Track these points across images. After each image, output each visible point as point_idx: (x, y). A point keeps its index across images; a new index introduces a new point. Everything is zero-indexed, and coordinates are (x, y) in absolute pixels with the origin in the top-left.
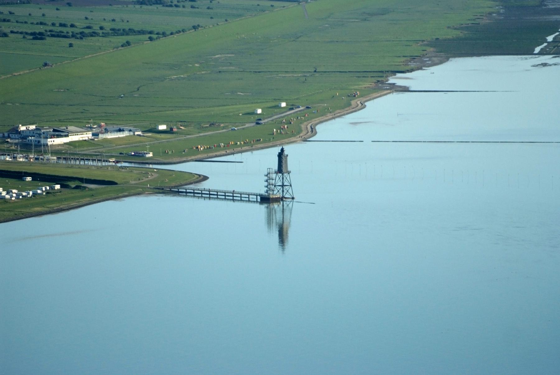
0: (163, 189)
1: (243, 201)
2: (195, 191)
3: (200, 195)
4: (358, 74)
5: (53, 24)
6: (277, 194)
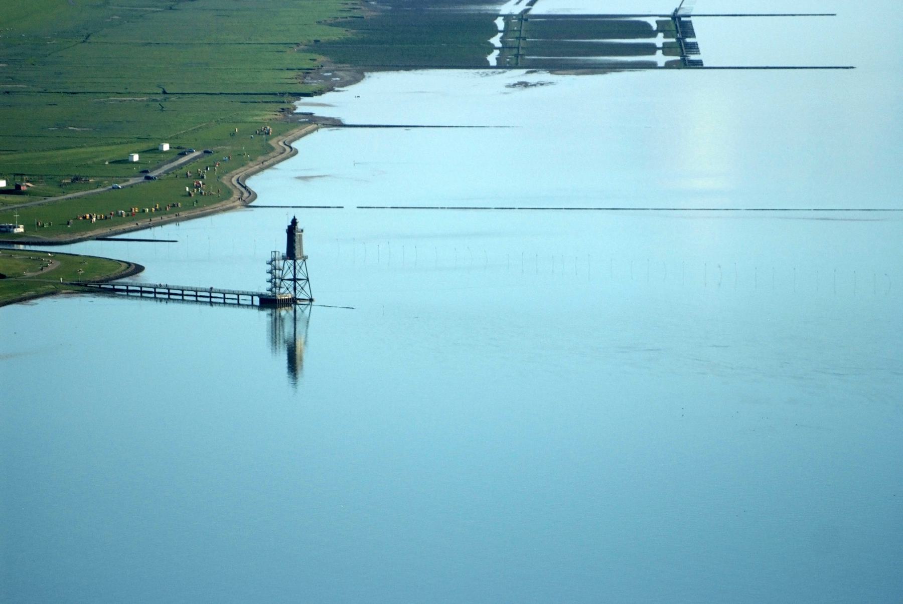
0: (86, 285)
2: (144, 289)
3: (153, 295)
4: (245, 98)
6: (285, 292)
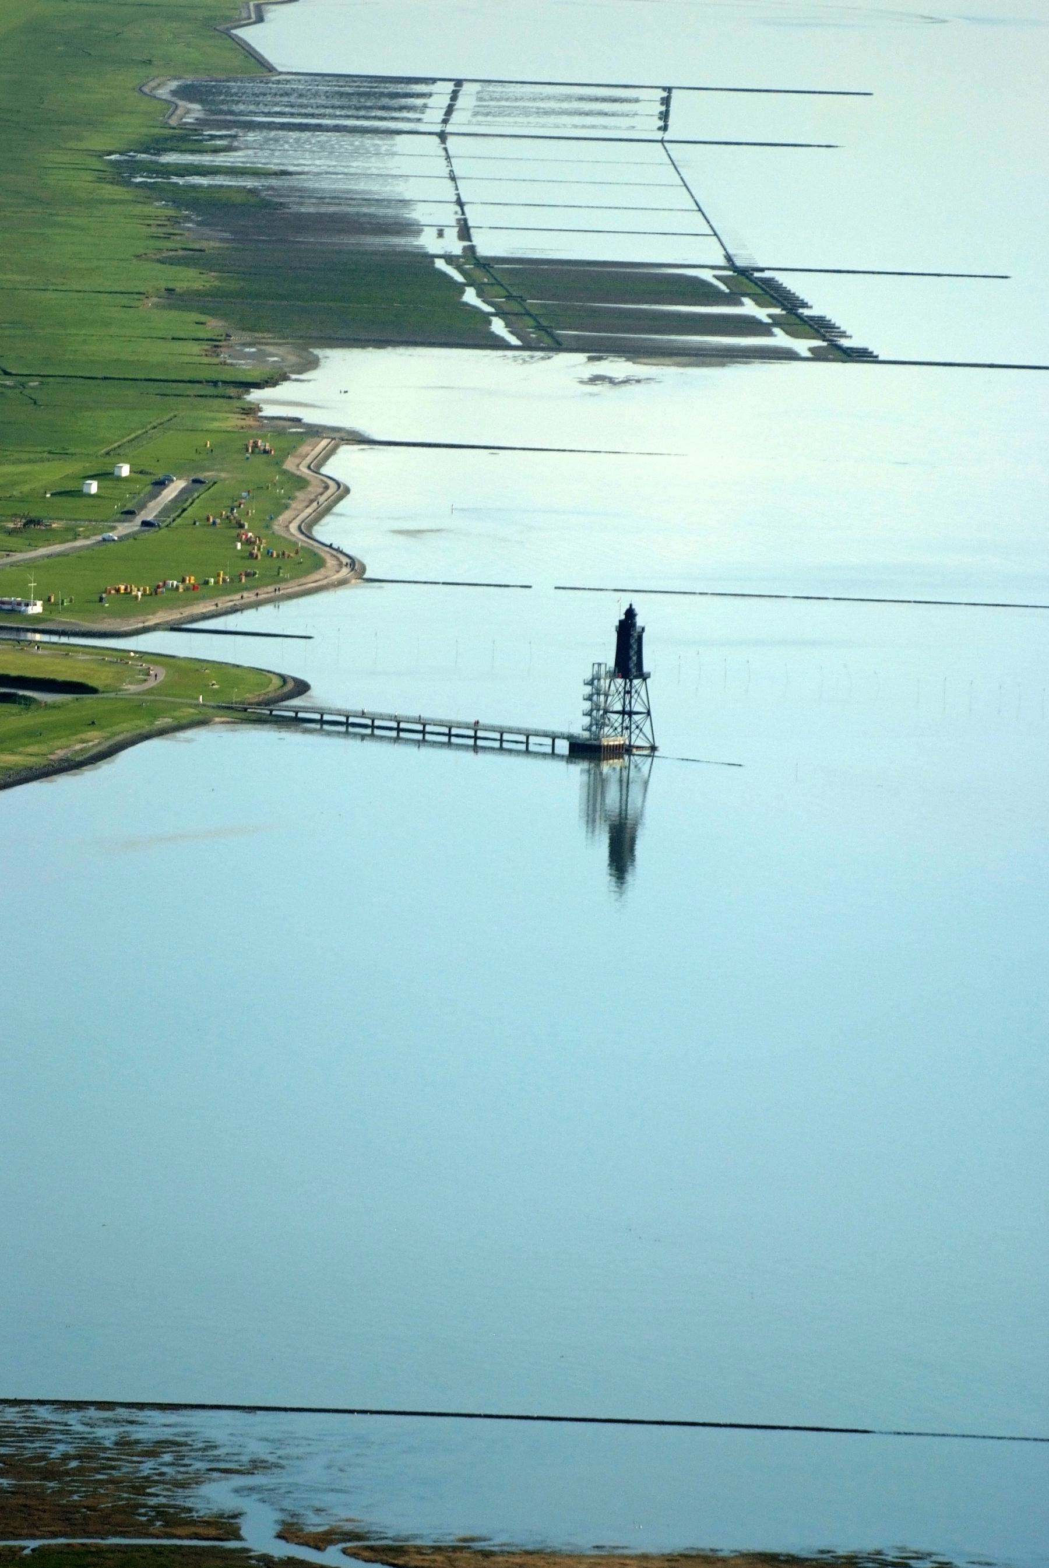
1: (510, 751)
3: (369, 731)
6: (611, 738)
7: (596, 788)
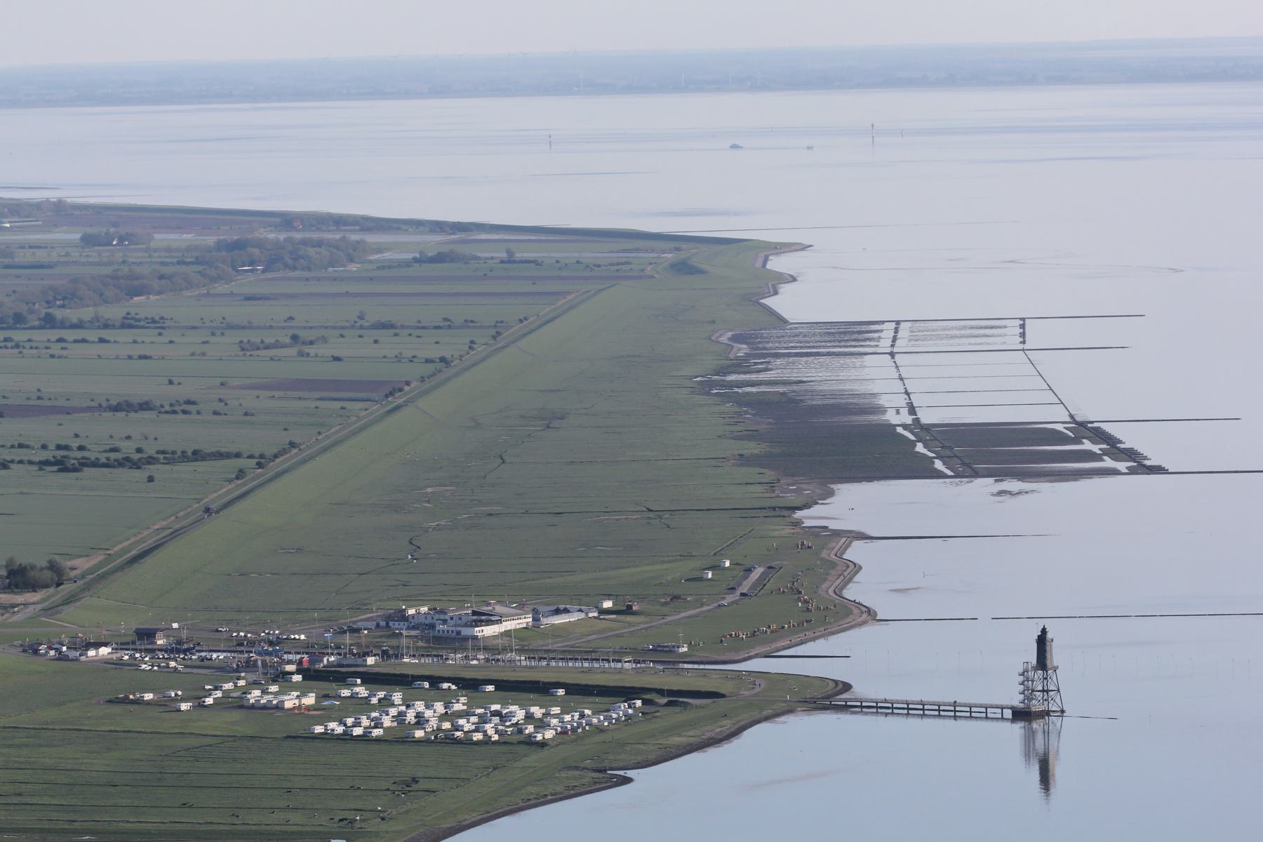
5: (44, 447)
6: (1036, 706)
7: (1030, 737)
